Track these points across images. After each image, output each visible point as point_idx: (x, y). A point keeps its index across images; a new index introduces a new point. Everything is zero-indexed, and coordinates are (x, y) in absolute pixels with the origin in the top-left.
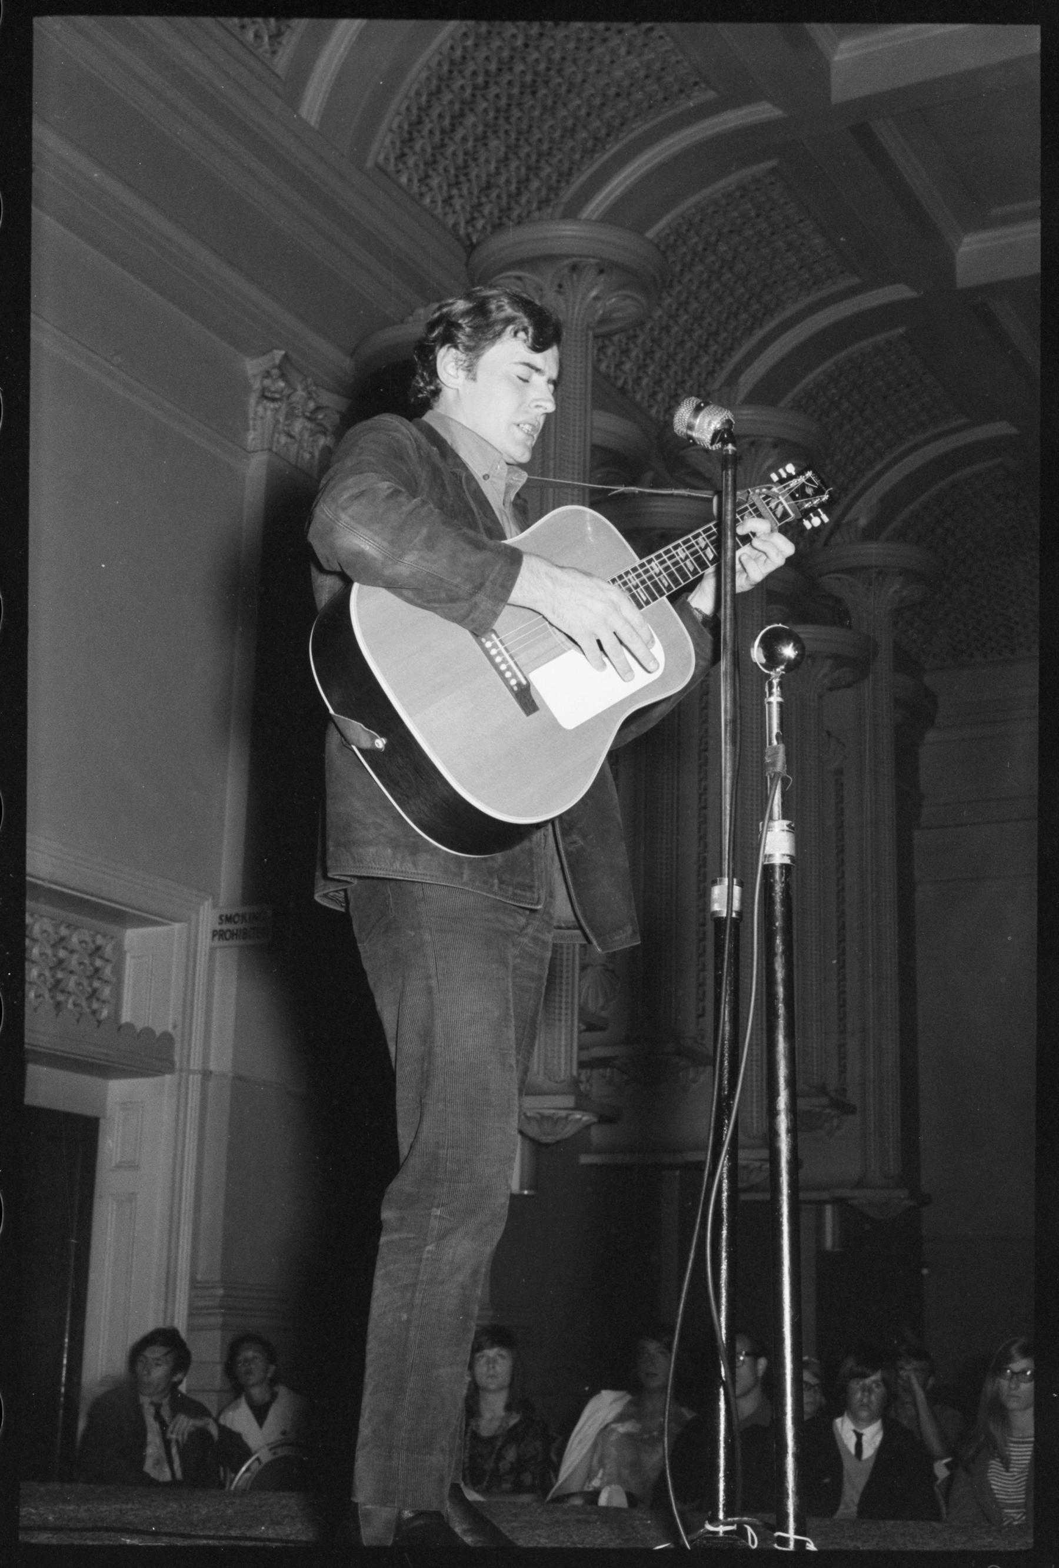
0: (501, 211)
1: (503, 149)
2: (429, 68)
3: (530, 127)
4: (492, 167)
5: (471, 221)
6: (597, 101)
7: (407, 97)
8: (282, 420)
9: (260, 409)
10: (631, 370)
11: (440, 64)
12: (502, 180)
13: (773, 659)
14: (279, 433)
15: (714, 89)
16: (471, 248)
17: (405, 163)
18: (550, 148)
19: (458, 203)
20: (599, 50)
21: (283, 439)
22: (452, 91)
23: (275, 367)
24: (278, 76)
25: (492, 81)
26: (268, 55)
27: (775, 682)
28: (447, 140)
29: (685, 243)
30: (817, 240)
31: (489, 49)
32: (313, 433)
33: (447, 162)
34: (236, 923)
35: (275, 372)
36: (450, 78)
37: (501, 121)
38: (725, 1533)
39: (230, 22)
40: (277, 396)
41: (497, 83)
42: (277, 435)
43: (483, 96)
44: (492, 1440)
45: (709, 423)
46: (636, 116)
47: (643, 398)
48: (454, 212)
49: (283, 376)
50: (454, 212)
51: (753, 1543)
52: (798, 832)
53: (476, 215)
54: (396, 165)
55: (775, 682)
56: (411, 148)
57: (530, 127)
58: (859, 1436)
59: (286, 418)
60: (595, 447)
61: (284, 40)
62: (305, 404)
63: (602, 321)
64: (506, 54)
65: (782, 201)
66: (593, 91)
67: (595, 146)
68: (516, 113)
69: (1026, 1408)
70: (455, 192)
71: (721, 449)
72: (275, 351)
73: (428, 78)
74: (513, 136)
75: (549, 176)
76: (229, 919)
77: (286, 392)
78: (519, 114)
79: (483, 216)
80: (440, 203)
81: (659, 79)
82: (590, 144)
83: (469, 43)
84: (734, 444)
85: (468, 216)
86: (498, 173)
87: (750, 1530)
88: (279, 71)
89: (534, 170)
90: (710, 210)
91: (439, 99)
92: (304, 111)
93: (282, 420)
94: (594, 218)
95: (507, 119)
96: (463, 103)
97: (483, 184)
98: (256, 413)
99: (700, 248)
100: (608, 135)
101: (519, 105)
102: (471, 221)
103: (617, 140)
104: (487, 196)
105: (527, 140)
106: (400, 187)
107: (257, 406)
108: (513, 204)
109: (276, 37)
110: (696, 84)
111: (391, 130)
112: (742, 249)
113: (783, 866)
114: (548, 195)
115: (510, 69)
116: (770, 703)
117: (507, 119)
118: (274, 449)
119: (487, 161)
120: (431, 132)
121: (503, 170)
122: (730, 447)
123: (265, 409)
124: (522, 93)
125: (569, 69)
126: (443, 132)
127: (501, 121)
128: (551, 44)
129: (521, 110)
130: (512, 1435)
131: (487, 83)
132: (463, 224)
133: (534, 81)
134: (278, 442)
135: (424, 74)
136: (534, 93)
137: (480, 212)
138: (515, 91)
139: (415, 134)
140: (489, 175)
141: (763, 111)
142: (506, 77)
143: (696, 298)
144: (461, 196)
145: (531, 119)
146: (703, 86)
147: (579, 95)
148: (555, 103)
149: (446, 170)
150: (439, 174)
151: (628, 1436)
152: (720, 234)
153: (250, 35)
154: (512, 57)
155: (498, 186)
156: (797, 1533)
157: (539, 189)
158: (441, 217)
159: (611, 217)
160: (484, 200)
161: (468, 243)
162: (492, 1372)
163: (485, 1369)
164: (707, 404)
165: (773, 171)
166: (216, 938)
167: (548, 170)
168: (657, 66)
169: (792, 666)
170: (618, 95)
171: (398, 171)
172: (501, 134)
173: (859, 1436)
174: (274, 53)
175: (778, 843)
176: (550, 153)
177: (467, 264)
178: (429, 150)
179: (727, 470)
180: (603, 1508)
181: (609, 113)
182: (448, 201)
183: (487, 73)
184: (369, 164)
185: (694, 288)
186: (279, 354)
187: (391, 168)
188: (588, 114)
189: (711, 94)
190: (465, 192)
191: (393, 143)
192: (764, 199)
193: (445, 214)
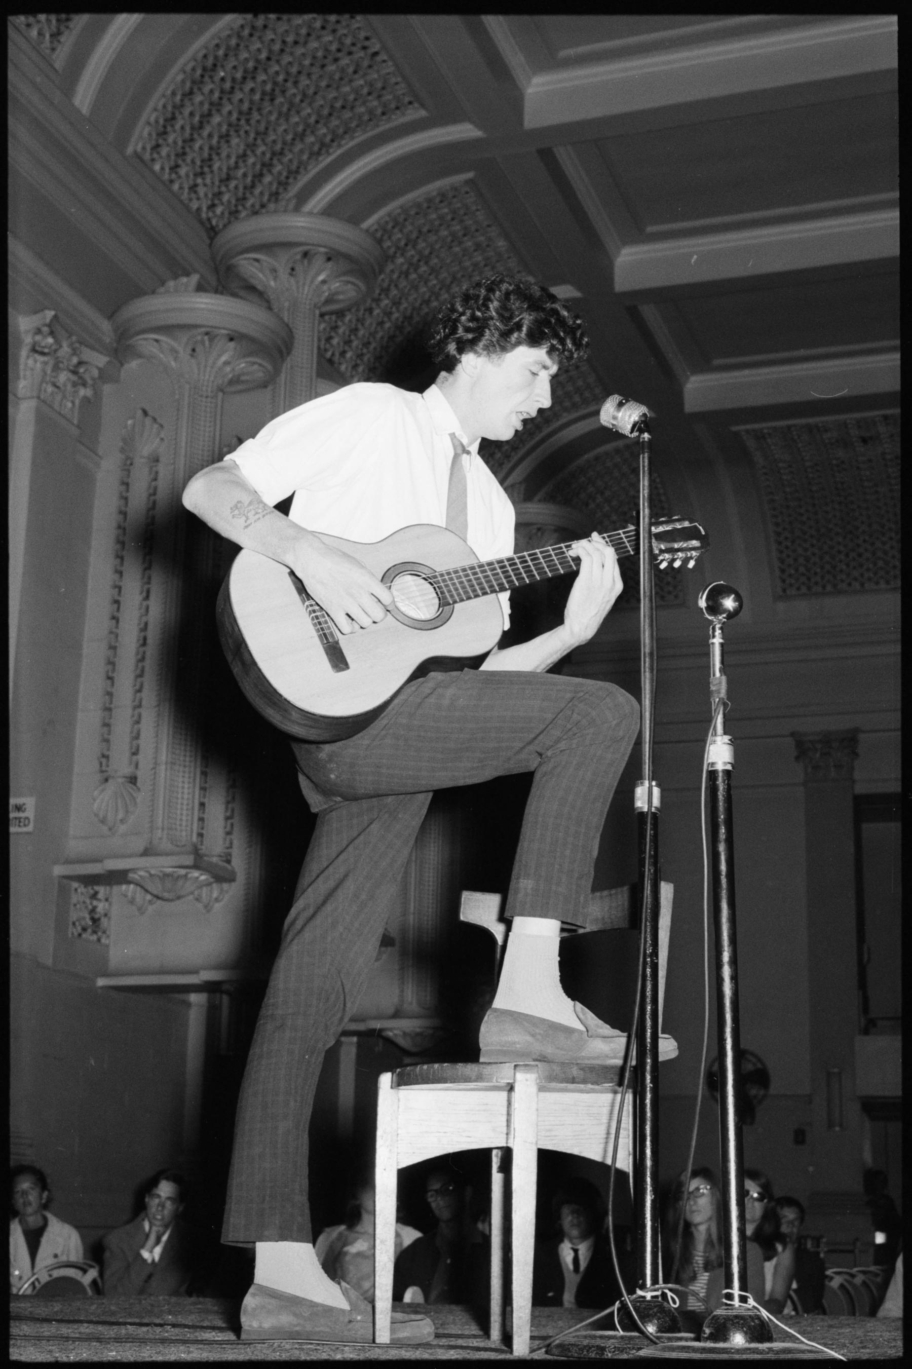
0: (237, 200)
1: (242, 147)
2: (185, 72)
3: (267, 129)
4: (233, 160)
5: (212, 206)
6: (326, 112)
7: (164, 96)
8: (49, 372)
9: (30, 362)
10: (338, 343)
11: (194, 69)
12: (240, 173)
13: (715, 608)
14: (47, 383)
15: (423, 106)
16: (213, 232)
17: (158, 153)
18: (282, 149)
19: (201, 191)
20: (332, 68)
21: (50, 389)
22: (203, 94)
23: (46, 325)
24: (56, 71)
25: (237, 87)
26: (48, 51)
27: (718, 626)
28: (196, 136)
29: (390, 238)
30: (501, 243)
31: (237, 59)
32: (75, 385)
33: (195, 155)
35: (46, 330)
36: (202, 82)
37: (243, 122)
38: (652, 1297)
39: (18, 21)
40: (46, 350)
41: (241, 89)
42: (44, 385)
43: (229, 99)
45: (630, 416)
46: (357, 126)
47: (347, 368)
48: (198, 199)
49: (52, 333)
50: (198, 199)
51: (674, 1302)
52: (736, 744)
53: (216, 202)
54: (151, 154)
55: (718, 626)
56: (165, 140)
57: (267, 129)
58: (576, 1251)
59: (53, 371)
61: (62, 39)
62: (69, 360)
63: (328, 301)
64: (251, 65)
65: (474, 208)
66: (322, 102)
67: (320, 149)
68: (256, 116)
69: (754, 1221)
70: (199, 181)
71: (639, 436)
72: (47, 312)
73: (183, 81)
74: (252, 135)
75: (280, 173)
77: (54, 347)
78: (259, 117)
79: (222, 204)
80: (186, 190)
81: (379, 97)
82: (316, 148)
83: (221, 53)
84: (649, 433)
85: (209, 203)
86: (237, 167)
87: (669, 1294)
88: (58, 65)
89: (267, 166)
90: (412, 212)
91: (190, 99)
92: (77, 101)
93: (49, 372)
94: (315, 211)
95: (248, 121)
96: (211, 104)
97: (224, 176)
98: (26, 364)
99: (403, 243)
100: (332, 141)
101: (259, 110)
102: (212, 206)
103: (340, 146)
104: (227, 186)
105: (263, 140)
106: (153, 172)
107: (28, 357)
108: (248, 195)
109: (56, 35)
110: (410, 103)
111: (149, 123)
112: (437, 246)
113: (727, 773)
114: (277, 188)
115: (254, 78)
116: (713, 644)
117: (248, 121)
118: (42, 397)
119: (229, 156)
120: (182, 128)
121: (241, 164)
122: (646, 436)
123: (36, 361)
124: (262, 99)
125: (304, 81)
126: (193, 128)
127: (243, 122)
128: (290, 59)
129: (261, 115)
131: (233, 88)
132: (204, 209)
133: (273, 90)
134: (45, 391)
135: (180, 77)
136: (272, 100)
137: (220, 200)
138: (257, 97)
139: (169, 129)
140: (229, 169)
141: (465, 131)
142: (250, 85)
143: (396, 286)
144: (205, 185)
145: (268, 122)
146: (416, 105)
147: (310, 104)
148: (289, 110)
149: (193, 162)
150: (187, 165)
152: (420, 232)
153: (34, 33)
154: (256, 68)
155: (236, 179)
156: (741, 1289)
157: (270, 183)
158: (186, 202)
159: (330, 211)
160: (223, 189)
161: (209, 226)
164: (627, 401)
165: (468, 182)
167: (279, 168)
168: (379, 85)
169: (731, 615)
170: (343, 107)
171: (153, 160)
172: (242, 133)
173: (576, 1251)
174: (53, 49)
175: (719, 753)
176: (282, 153)
177: (210, 245)
178: (180, 143)
179: (643, 453)
180: (408, 1304)
181: (335, 122)
182: (193, 188)
183: (234, 80)
184: (130, 150)
185: (395, 276)
186: (50, 314)
187: (147, 156)
188: (317, 122)
189: (423, 113)
190: (208, 181)
191: (150, 134)
192: (459, 205)
193: (191, 200)
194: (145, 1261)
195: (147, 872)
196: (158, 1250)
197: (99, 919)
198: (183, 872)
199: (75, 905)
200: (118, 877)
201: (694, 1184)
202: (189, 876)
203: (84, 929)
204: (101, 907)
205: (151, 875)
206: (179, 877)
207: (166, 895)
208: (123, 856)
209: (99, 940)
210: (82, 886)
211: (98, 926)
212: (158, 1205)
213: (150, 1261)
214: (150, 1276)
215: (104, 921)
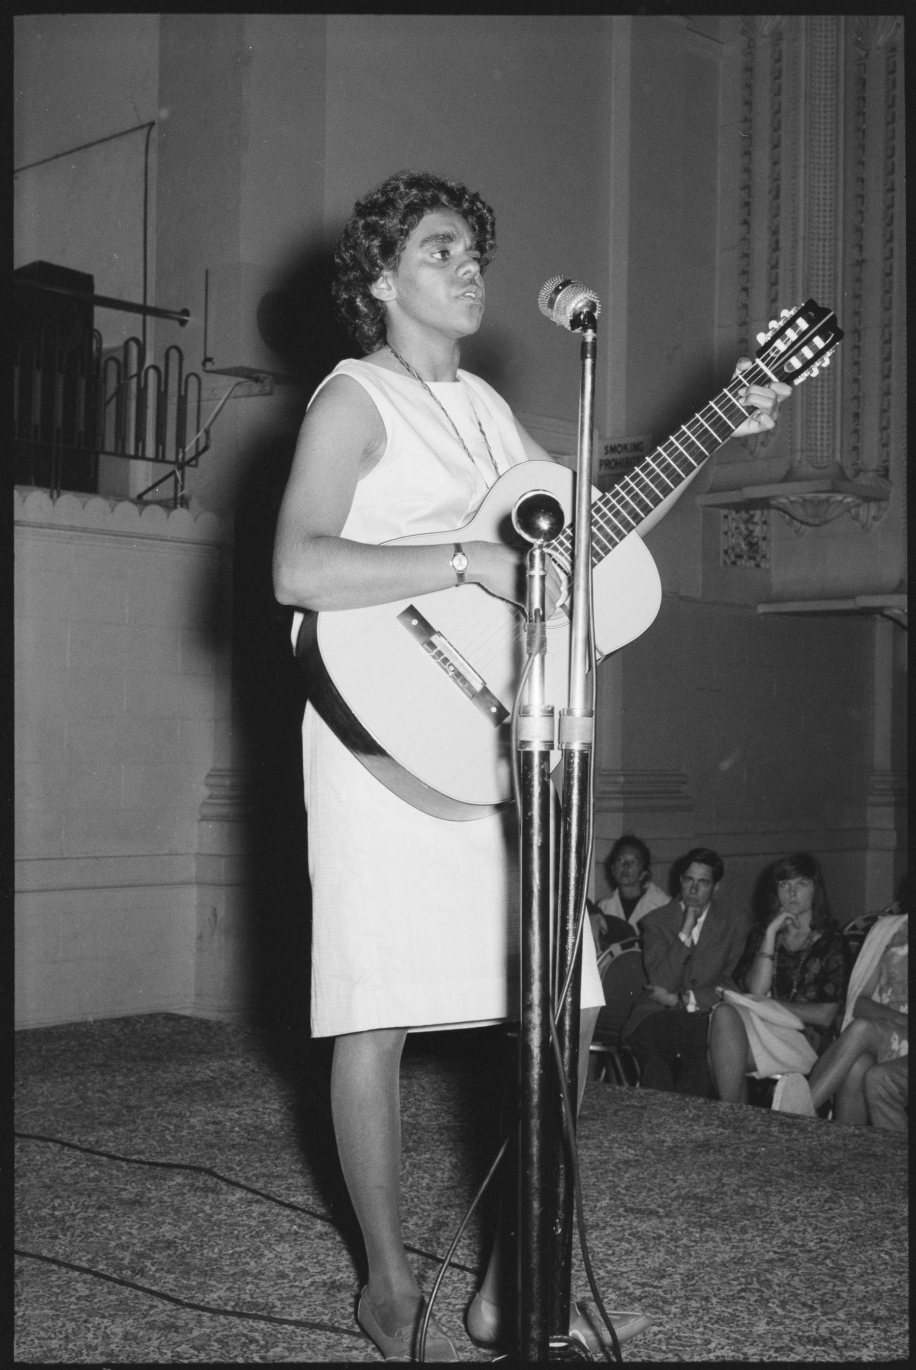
34: (619, 453)
44: (798, 953)
60: (545, 742)
76: (613, 449)
130: (816, 951)
151: (641, 1086)
162: (793, 899)
163: (788, 896)
166: (603, 467)
194: (683, 943)
195: (787, 498)
196: (696, 932)
197: (757, 543)
198: (823, 496)
199: (726, 533)
200: (764, 503)
201: (570, 1334)
202: (832, 500)
203: (739, 556)
204: (758, 531)
205: (791, 502)
206: (821, 502)
207: (811, 520)
208: (767, 483)
209: (758, 566)
210: (733, 513)
211: (756, 552)
212: (692, 887)
213: (688, 944)
214: (688, 958)
215: (763, 545)
